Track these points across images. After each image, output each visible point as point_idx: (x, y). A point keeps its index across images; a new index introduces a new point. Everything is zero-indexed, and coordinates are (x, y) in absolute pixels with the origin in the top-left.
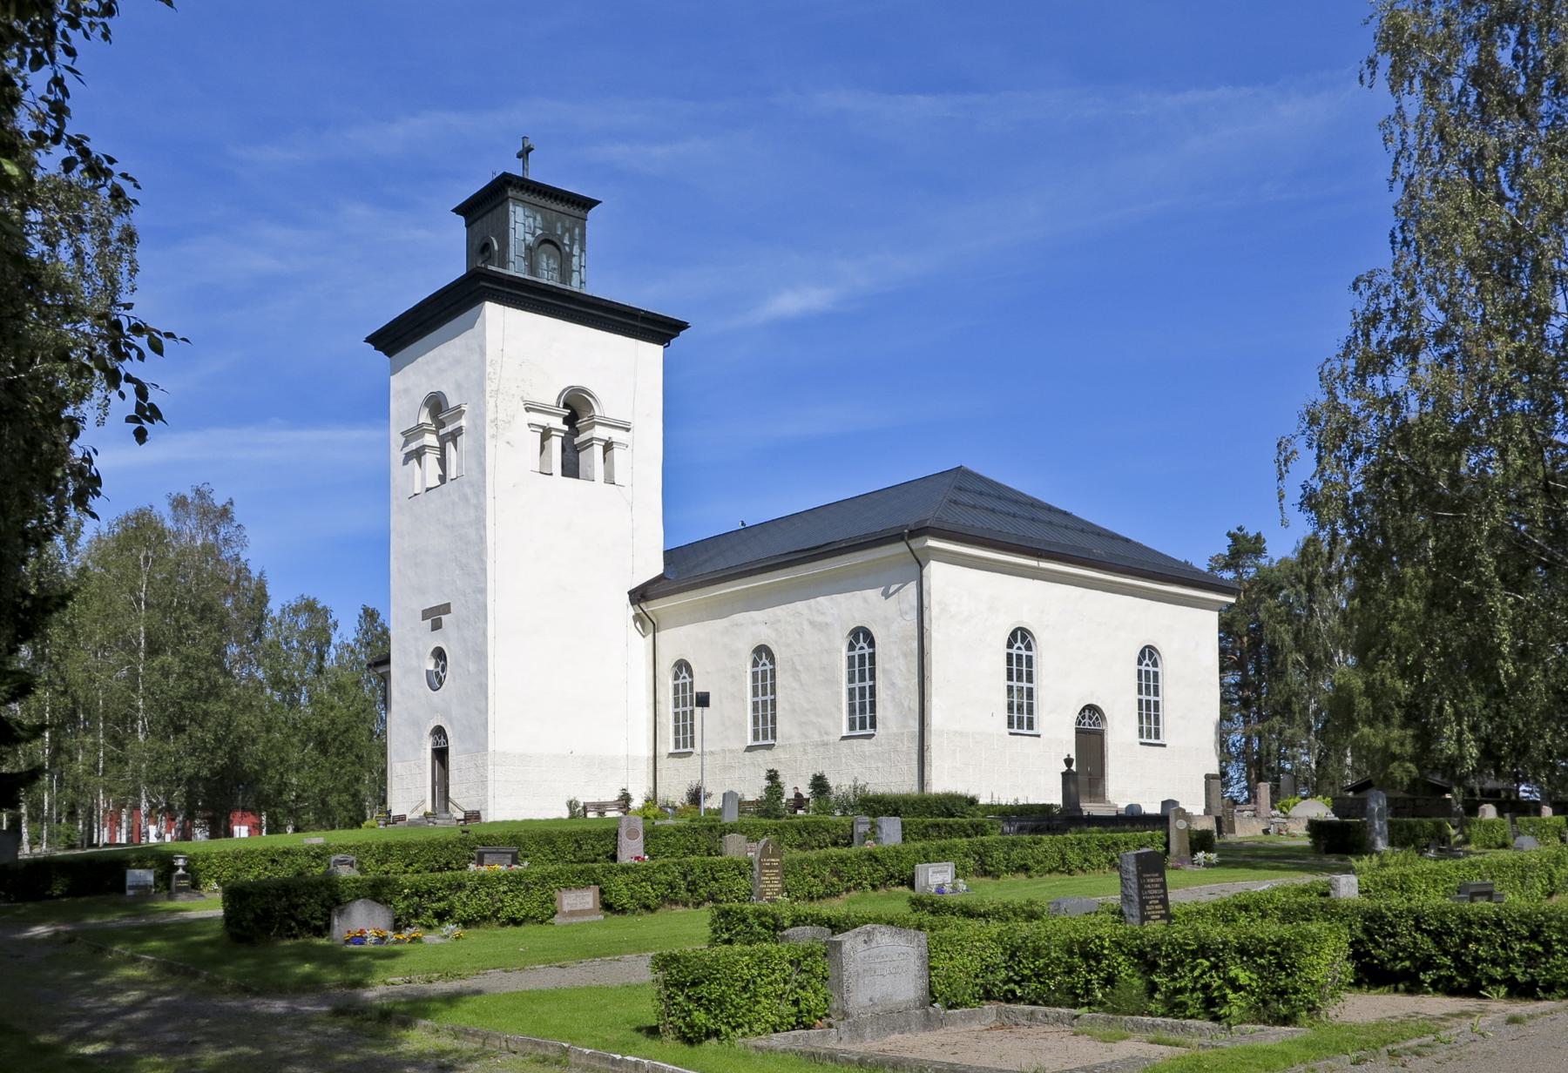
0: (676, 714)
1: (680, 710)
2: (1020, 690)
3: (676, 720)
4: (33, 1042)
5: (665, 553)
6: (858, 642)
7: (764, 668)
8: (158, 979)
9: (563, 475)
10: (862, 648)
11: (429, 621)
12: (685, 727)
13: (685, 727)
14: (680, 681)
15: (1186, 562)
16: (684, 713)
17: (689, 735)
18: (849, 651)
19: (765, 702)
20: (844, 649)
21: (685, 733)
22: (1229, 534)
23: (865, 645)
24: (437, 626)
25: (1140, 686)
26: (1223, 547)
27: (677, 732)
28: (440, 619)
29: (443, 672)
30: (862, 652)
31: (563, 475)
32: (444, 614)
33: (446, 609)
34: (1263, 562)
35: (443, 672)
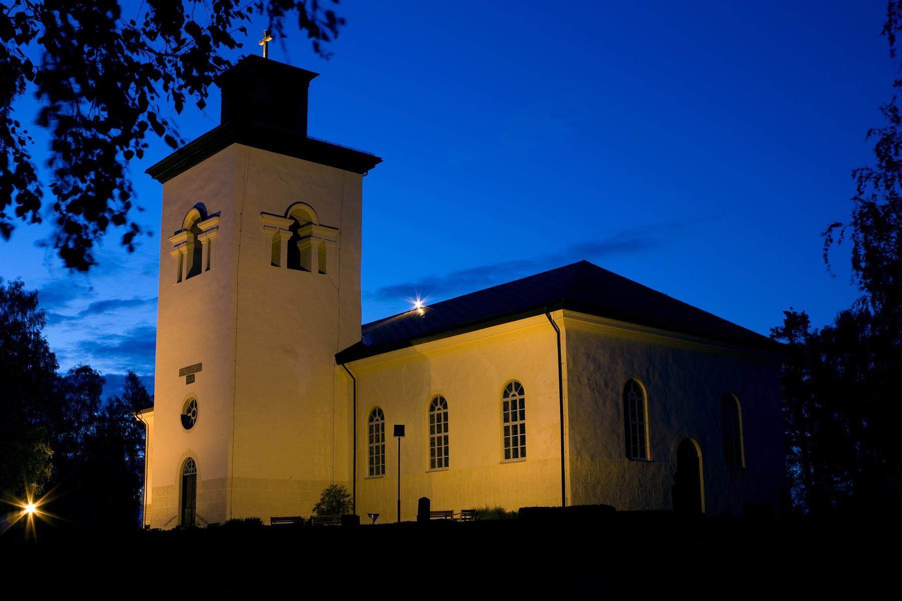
1: (380, 444)
2: (377, 447)
3: (371, 453)
4: (52, 12)
5: (153, 406)
6: (437, 405)
7: (377, 423)
9: (289, 267)
11: (184, 378)
12: (377, 458)
13: (377, 458)
14: (374, 423)
16: (377, 447)
20: (427, 408)
21: (378, 462)
23: (516, 393)
24: (190, 380)
25: (383, 452)
26: (780, 322)
30: (514, 398)
31: (289, 267)
32: (196, 372)
35: (194, 416)
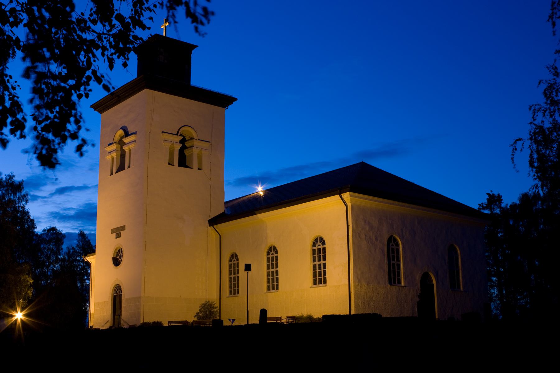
0: (230, 278)
2: (234, 278)
3: (230, 281)
6: (271, 251)
7: (234, 262)
8: (57, 63)
10: (319, 245)
11: (114, 234)
12: (234, 284)
13: (234, 284)
14: (232, 263)
15: (502, 200)
17: (236, 288)
18: (267, 255)
19: (273, 272)
20: (265, 253)
21: (235, 287)
22: (488, 194)
23: (321, 244)
24: (118, 236)
25: (238, 280)
26: (484, 200)
27: (230, 287)
28: (120, 233)
29: (120, 258)
32: (122, 231)
33: (123, 228)
34: (503, 205)
